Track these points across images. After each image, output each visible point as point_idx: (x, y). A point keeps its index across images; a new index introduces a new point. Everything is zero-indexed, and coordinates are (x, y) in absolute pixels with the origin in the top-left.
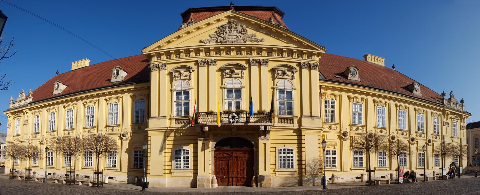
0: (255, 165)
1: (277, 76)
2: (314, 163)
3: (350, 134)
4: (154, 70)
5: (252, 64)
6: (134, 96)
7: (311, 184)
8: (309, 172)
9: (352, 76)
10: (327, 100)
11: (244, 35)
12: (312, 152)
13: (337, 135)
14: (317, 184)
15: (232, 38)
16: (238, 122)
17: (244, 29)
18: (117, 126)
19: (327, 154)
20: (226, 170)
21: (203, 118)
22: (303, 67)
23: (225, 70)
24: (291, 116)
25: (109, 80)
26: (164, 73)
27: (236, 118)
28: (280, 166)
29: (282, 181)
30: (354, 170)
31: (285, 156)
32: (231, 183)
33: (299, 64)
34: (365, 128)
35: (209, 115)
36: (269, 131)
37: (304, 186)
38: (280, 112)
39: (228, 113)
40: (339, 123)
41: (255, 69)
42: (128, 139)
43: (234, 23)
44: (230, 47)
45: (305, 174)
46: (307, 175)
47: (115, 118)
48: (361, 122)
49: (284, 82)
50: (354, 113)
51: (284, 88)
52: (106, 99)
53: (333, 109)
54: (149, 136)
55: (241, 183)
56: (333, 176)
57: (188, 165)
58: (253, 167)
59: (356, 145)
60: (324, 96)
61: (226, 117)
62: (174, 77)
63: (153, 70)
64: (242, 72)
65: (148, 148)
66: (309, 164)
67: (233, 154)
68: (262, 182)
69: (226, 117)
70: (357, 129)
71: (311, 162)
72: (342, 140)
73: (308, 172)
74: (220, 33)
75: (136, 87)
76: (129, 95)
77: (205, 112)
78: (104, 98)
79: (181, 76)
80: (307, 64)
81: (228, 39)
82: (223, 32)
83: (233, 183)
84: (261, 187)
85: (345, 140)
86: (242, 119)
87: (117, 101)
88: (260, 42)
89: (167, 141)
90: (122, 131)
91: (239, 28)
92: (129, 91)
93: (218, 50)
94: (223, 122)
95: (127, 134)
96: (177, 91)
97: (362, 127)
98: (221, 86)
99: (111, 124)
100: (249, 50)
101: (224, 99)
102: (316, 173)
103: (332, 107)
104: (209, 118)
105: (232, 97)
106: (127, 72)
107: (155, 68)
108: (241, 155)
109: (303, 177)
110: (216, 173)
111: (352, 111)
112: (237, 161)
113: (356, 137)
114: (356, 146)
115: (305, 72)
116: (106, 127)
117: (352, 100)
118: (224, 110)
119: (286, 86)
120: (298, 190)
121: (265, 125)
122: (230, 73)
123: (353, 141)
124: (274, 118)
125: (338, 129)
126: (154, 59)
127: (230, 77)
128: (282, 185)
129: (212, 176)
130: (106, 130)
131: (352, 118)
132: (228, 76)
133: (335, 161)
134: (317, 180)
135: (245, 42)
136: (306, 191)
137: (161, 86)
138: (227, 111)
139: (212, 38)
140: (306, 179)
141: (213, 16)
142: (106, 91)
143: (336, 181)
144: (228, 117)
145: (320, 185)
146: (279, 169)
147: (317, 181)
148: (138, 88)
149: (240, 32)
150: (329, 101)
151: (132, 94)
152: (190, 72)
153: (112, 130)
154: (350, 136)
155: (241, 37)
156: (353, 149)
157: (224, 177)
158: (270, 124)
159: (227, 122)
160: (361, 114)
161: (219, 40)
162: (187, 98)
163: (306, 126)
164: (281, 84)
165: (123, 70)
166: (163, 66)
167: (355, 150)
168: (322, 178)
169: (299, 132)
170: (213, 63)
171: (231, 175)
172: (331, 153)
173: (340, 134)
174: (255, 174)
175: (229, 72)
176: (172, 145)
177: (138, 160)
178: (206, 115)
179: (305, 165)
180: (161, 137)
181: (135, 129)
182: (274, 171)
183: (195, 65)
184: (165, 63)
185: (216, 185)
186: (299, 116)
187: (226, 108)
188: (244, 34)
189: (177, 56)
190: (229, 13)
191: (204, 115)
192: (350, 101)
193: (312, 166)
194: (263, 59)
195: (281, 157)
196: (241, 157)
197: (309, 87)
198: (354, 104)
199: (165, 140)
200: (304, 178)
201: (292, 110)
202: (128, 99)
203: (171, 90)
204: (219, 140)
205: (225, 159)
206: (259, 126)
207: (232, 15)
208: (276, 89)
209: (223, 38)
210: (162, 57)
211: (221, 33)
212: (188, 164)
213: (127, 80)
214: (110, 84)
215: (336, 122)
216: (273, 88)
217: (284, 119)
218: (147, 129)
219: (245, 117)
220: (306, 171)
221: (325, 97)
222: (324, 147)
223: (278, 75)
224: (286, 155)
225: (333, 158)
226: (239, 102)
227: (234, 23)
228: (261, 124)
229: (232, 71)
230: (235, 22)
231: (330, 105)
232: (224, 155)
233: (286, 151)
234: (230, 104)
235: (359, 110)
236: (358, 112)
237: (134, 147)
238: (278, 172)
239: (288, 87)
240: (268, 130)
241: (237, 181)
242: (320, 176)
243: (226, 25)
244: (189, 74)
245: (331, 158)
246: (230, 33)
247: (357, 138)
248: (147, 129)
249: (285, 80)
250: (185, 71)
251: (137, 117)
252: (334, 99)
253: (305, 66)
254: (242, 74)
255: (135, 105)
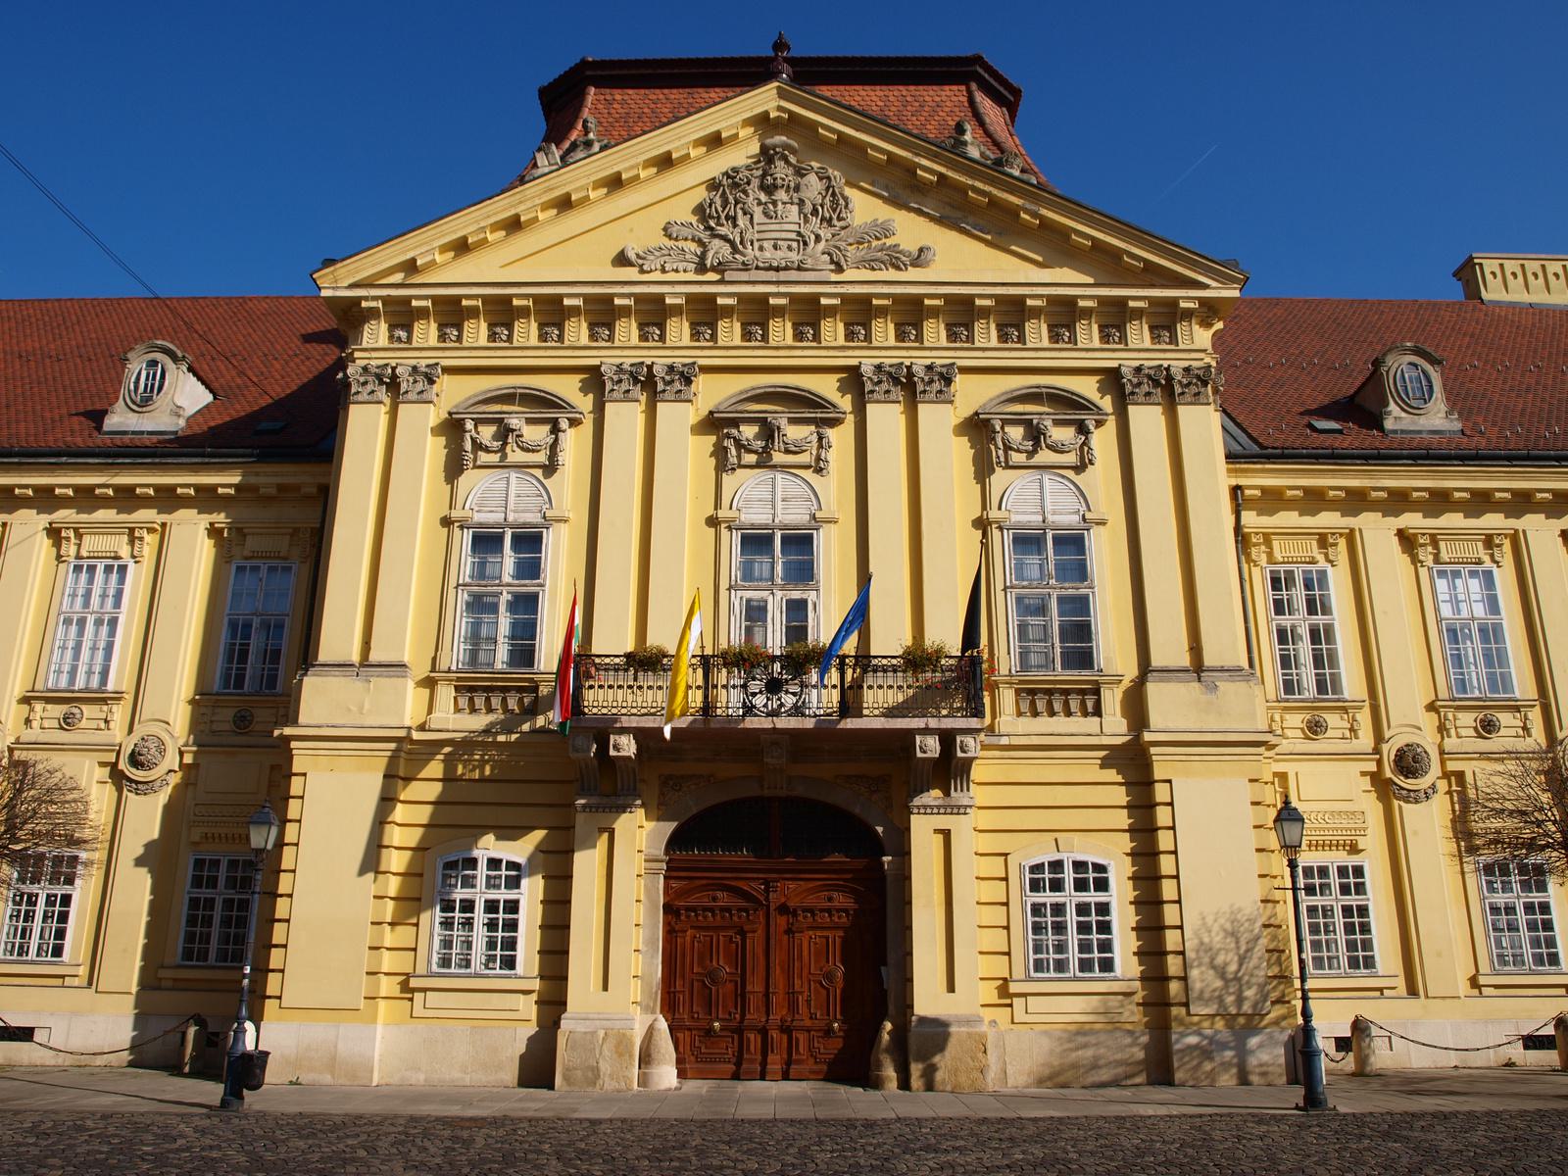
0: (892, 957)
1: (1001, 452)
2: (1237, 942)
3: (1443, 763)
4: (364, 397)
5: (872, 392)
6: (229, 529)
7: (1226, 1077)
8: (1207, 995)
9: (1407, 407)
10: (1282, 568)
11: (832, 230)
12: (1221, 876)
13: (1363, 774)
14: (1264, 1074)
15: (775, 247)
16: (798, 711)
17: (834, 194)
18: (104, 701)
19: (1310, 890)
20: (730, 986)
21: (611, 687)
22: (1133, 393)
23: (738, 427)
24: (1085, 675)
25: (97, 417)
26: (421, 420)
27: (787, 692)
28: (1036, 961)
29: (1051, 1052)
30: (1496, 987)
31: (1064, 905)
32: (752, 1061)
33: (1112, 379)
34: (1535, 716)
35: (645, 671)
36: (968, 764)
37: (1182, 1085)
38: (1024, 655)
39: (744, 660)
40: (1365, 696)
41: (886, 419)
42: (165, 782)
43: (787, 162)
44: (767, 296)
45: (1183, 1010)
46: (1196, 1019)
47: (94, 648)
48: (1506, 680)
49: (1041, 487)
50: (1452, 632)
51: (1040, 518)
52: (59, 530)
53: (1320, 619)
54: (295, 770)
55: (810, 1065)
56: (1360, 1026)
57: (514, 949)
58: (883, 968)
59: (1496, 824)
60: (1263, 548)
61: (734, 687)
62: (468, 446)
63: (360, 398)
64: (820, 438)
65: (280, 844)
66: (1204, 947)
67: (767, 890)
68: (937, 1059)
69: (734, 687)
70: (1488, 727)
71: (1217, 939)
72: (1396, 803)
73: (1200, 998)
74: (719, 217)
75: (253, 480)
76: (204, 521)
77: (625, 655)
78: (44, 520)
79: (505, 444)
80: (1152, 372)
81: (758, 253)
82: (732, 213)
83: (764, 1063)
84: (930, 1086)
85: (1412, 797)
86: (823, 698)
87: (125, 551)
88: (913, 265)
89: (399, 805)
90: (131, 731)
91: (813, 186)
92: (206, 499)
93: (705, 314)
94: (719, 712)
95: (162, 751)
96: (481, 525)
97: (1517, 709)
98: (711, 511)
99: (63, 683)
100: (860, 313)
101: (724, 584)
102: (1255, 1006)
103: (1312, 609)
104: (640, 688)
105: (766, 574)
106: (215, 385)
107: (369, 387)
108: (810, 901)
109: (1176, 1028)
110: (670, 1003)
111: (1439, 620)
112: (789, 931)
113: (1484, 776)
114: (1498, 832)
115: (1147, 420)
116: (26, 700)
117: (1426, 555)
118: (724, 645)
119: (1049, 507)
120: (1150, 1110)
121: (946, 730)
122: (759, 444)
123: (1465, 801)
124: (994, 687)
125: (1360, 733)
126: (376, 334)
127: (758, 466)
128: (1055, 1078)
129: (649, 1019)
130: (28, 721)
131: (1445, 660)
132: (751, 458)
133: (1365, 928)
134: (1260, 1046)
135: (839, 269)
136: (1201, 1116)
137: (396, 500)
138: (741, 653)
139: (680, 244)
140: (1193, 1040)
141: (690, 114)
142: (64, 481)
143: (1383, 1056)
144: (744, 686)
145: (1284, 1079)
146: (1029, 979)
147: (1264, 1056)
148: (262, 491)
149: (815, 212)
150: (1290, 574)
151: (220, 518)
152: (556, 430)
153: (67, 722)
154: (1446, 775)
155: (818, 238)
156: (1472, 850)
157: (716, 1024)
158: (974, 723)
159: (741, 712)
160: (1498, 629)
161: (710, 255)
162: (530, 569)
163: (1172, 726)
164: (1028, 496)
165: (190, 369)
166: (415, 382)
167: (1489, 860)
168: (1292, 1038)
169: (1133, 763)
170: (677, 386)
171: (754, 1016)
172: (1334, 880)
173: (1379, 762)
174: (891, 1009)
175: (757, 437)
176: (429, 809)
177: (40, 908)
178: (626, 670)
179: (1182, 953)
180: (372, 783)
181: (215, 727)
182: (1004, 990)
183: (584, 390)
184: (428, 366)
185: (666, 1075)
186: (1130, 671)
187: (733, 636)
188: (835, 222)
189: (498, 330)
190: (765, 99)
191: (616, 670)
192: (1415, 561)
193: (1226, 964)
194: (928, 362)
195: (1037, 909)
196: (812, 911)
197: (1172, 505)
198: (1442, 574)
199: (387, 801)
200: (1183, 1035)
201: (1090, 640)
202: (193, 547)
203: (446, 522)
204: (695, 811)
205: (723, 917)
206: (910, 734)
207: (780, 108)
208: (1001, 529)
209: (732, 243)
210: (418, 327)
211: (723, 216)
212: (511, 944)
213: (204, 433)
214: (99, 439)
215: (1346, 695)
216: (982, 524)
217: (1049, 692)
218: (288, 731)
219: (834, 687)
220: (1193, 995)
221: (1270, 554)
222: (1291, 849)
223: (1007, 448)
224: (1070, 897)
225: (1347, 911)
226: (805, 602)
227: (787, 162)
228: (923, 726)
229: (769, 432)
230: (794, 151)
231: (1299, 594)
232: (719, 894)
233: (1069, 876)
234: (755, 613)
235: (1479, 610)
236: (1473, 619)
237: (196, 835)
238: (1024, 995)
239: (1063, 512)
240: (960, 754)
241: (790, 1054)
242: (1276, 1022)
243: (748, 168)
244: (550, 439)
245: (1338, 912)
246: (766, 214)
247: (1497, 779)
248: (288, 731)
249: (1046, 478)
250: (530, 421)
251: (238, 654)
252: (1320, 558)
253: (1145, 388)
254: (820, 446)
255: (230, 589)
